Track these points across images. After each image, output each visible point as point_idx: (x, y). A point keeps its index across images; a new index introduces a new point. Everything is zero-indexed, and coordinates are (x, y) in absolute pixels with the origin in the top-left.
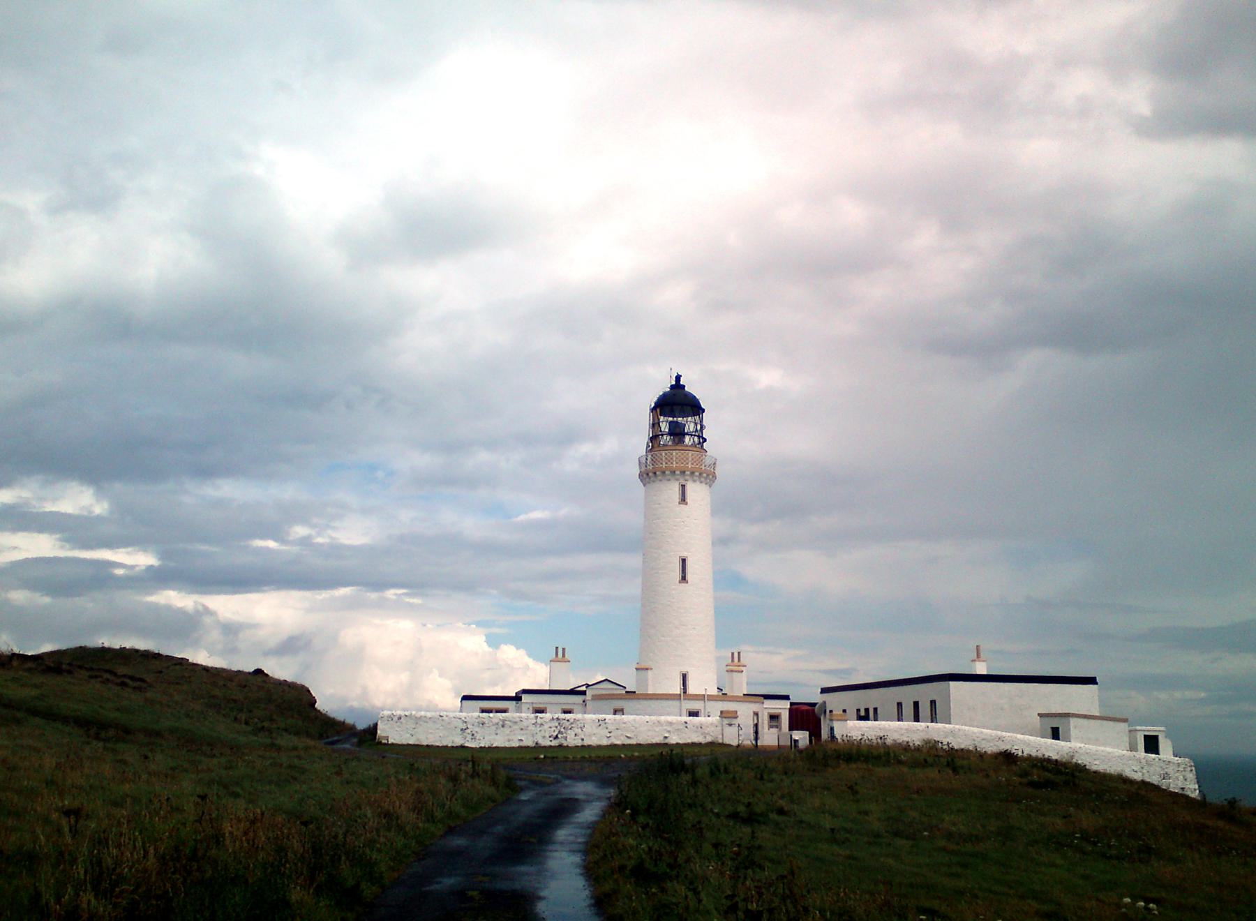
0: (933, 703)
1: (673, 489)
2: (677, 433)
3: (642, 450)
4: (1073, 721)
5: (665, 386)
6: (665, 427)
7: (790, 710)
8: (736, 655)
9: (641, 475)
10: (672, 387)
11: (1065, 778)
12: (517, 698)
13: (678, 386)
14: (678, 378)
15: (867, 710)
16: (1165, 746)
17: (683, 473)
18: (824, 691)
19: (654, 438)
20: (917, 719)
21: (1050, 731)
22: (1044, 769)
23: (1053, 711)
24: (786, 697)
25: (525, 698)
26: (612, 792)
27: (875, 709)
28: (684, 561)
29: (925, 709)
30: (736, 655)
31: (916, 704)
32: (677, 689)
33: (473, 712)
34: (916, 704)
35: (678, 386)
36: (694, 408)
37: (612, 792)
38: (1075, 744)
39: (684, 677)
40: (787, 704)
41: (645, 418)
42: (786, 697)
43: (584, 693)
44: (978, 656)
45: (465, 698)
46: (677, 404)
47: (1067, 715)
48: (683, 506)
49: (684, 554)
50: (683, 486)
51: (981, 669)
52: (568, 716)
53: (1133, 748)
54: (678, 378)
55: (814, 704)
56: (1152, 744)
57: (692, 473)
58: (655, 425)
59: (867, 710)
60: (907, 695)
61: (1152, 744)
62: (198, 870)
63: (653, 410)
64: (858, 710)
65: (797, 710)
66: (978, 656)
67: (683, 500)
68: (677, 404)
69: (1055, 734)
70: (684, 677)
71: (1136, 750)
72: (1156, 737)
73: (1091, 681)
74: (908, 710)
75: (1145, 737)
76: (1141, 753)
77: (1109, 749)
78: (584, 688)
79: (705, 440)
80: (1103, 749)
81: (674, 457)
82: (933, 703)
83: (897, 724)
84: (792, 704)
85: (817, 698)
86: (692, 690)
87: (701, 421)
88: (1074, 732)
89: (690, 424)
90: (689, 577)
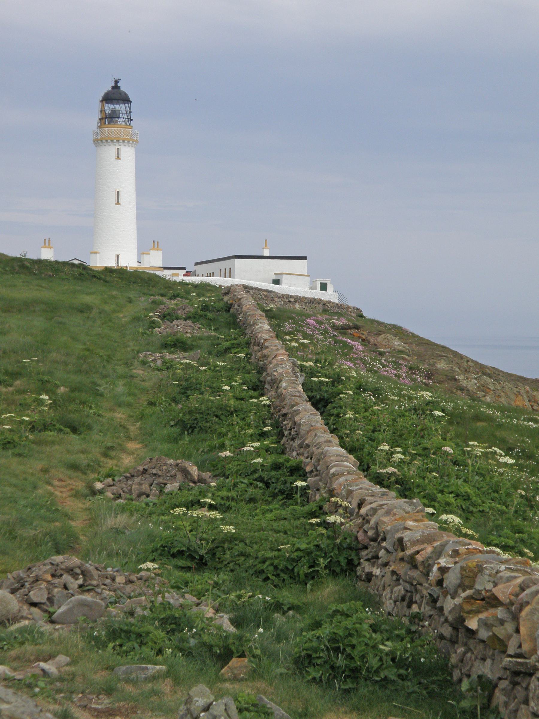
1: (111, 150)
4: (284, 276)
8: (47, 241)
9: (94, 141)
10: (113, 88)
13: (116, 87)
14: (116, 82)
16: (330, 287)
17: (118, 141)
18: (196, 264)
24: (184, 268)
27: (49, 240)
28: (118, 192)
30: (47, 241)
35: (116, 87)
36: (126, 100)
39: (118, 257)
42: (184, 268)
44: (266, 246)
46: (115, 96)
47: (282, 274)
48: (118, 160)
49: (118, 188)
50: (118, 149)
51: (266, 253)
52: (307, 415)
56: (324, 287)
57: (124, 141)
61: (324, 287)
63: (102, 101)
66: (266, 246)
67: (118, 157)
68: (115, 96)
70: (118, 257)
71: (316, 289)
73: (305, 258)
76: (318, 290)
77: (299, 289)
81: (111, 131)
87: (130, 108)
88: (236, 272)
89: (121, 107)
90: (121, 201)
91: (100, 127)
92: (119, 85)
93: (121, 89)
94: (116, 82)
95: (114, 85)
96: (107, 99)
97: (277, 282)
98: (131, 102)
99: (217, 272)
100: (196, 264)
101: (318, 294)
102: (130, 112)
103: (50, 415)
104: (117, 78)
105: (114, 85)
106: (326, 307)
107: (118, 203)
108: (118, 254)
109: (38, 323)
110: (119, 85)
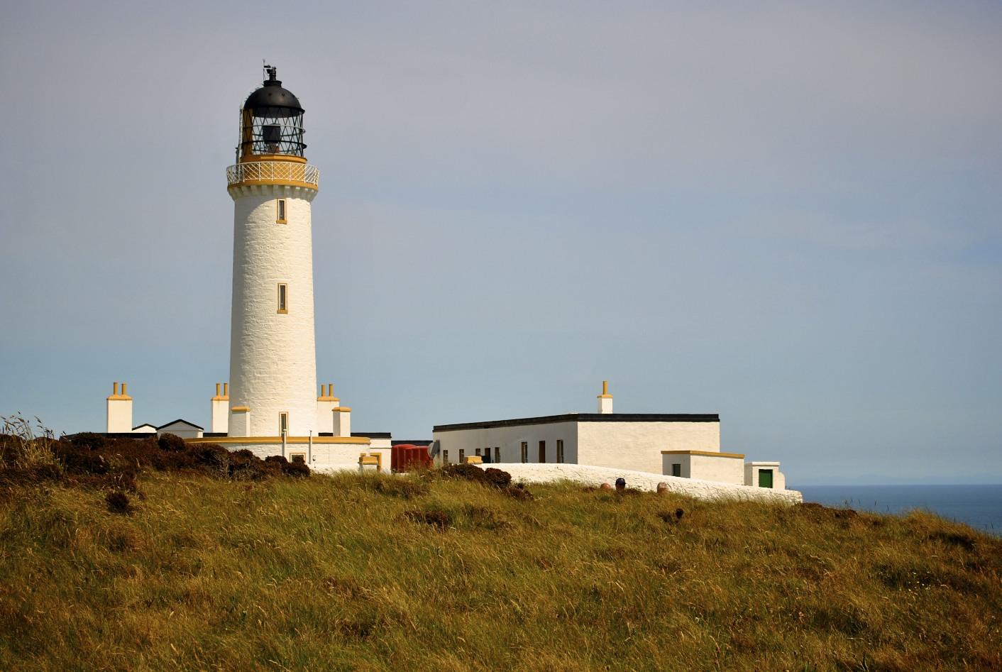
1: (270, 208)
2: (272, 136)
3: (231, 159)
4: (692, 458)
5: (257, 82)
7: (394, 451)
9: (230, 187)
10: (266, 83)
11: (680, 515)
13: (272, 83)
15: (488, 450)
16: (779, 480)
19: (246, 144)
20: (542, 460)
21: (671, 468)
22: (498, 475)
23: (705, 457)
24: (387, 436)
27: (497, 449)
29: (551, 449)
31: (542, 444)
32: (275, 432)
34: (542, 444)
35: (272, 83)
36: (294, 109)
40: (387, 443)
42: (387, 436)
46: (270, 103)
47: (688, 452)
49: (283, 281)
50: (282, 203)
51: (607, 407)
53: (748, 481)
54: (272, 72)
55: (428, 443)
58: (247, 128)
59: (488, 450)
60: (532, 435)
61: (766, 478)
62: (656, 619)
65: (401, 450)
67: (282, 217)
68: (270, 103)
70: (284, 417)
72: (770, 472)
73: (714, 418)
74: (534, 450)
75: (761, 471)
79: (305, 146)
80: (716, 479)
84: (393, 443)
85: (429, 436)
86: (292, 431)
89: (286, 125)
91: (243, 159)
93: (283, 86)
95: (268, 79)
96: (257, 104)
97: (677, 471)
98: (303, 111)
101: (755, 490)
102: (301, 131)
106: (779, 514)
107: (283, 306)
108: (283, 411)
110: (278, 78)
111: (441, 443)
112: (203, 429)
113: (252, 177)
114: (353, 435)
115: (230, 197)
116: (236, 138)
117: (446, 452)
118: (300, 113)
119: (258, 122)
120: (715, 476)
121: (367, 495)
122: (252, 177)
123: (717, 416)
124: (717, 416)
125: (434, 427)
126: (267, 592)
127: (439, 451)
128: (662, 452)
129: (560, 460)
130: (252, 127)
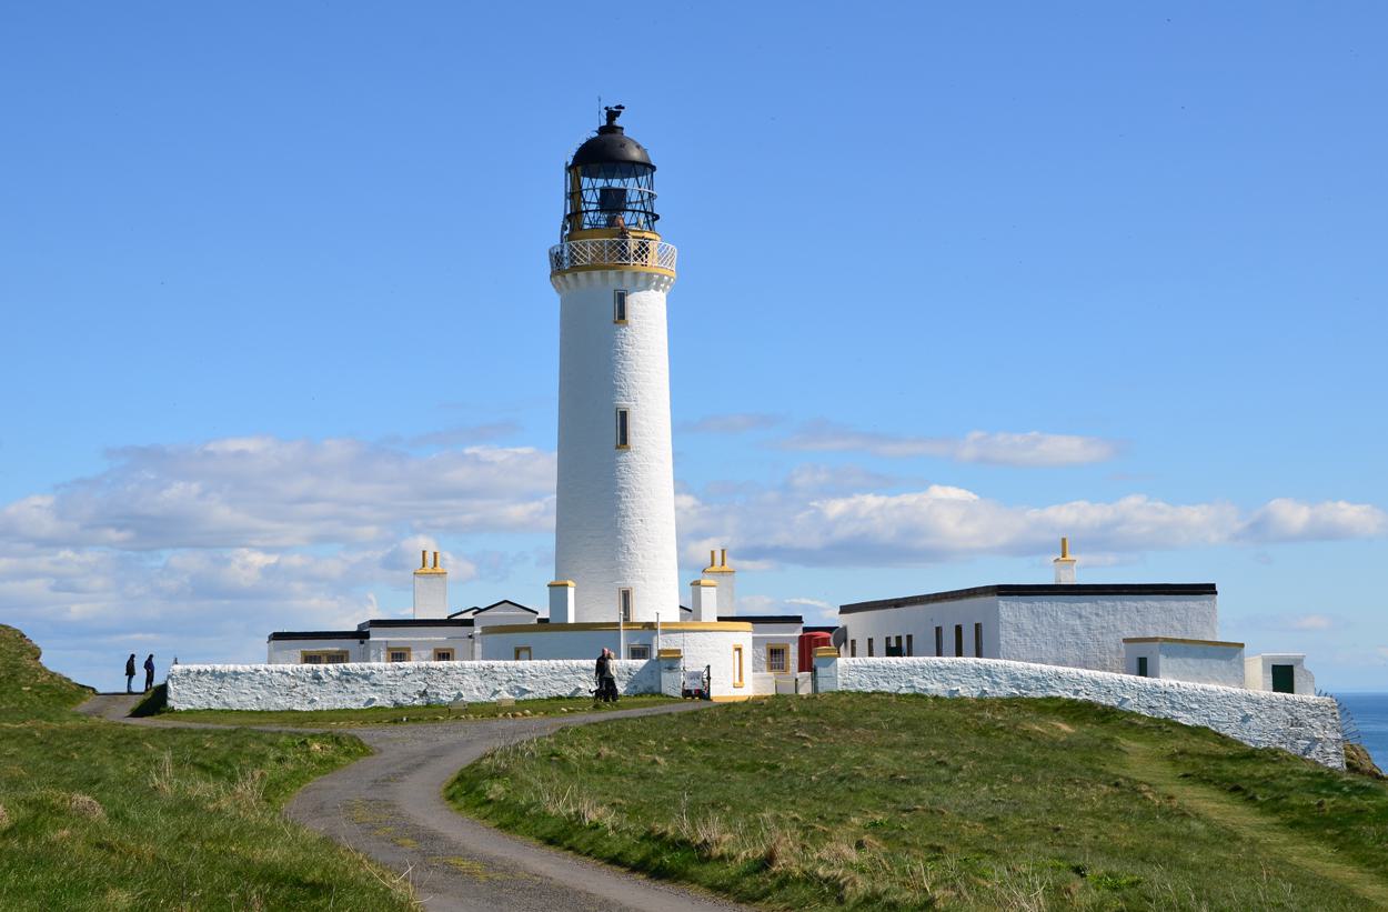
0: (978, 626)
2: (613, 202)
5: (589, 131)
6: (591, 198)
10: (602, 130)
12: (361, 635)
13: (609, 129)
14: (612, 115)
15: (899, 639)
18: (845, 610)
19: (574, 217)
20: (959, 653)
24: (798, 620)
25: (377, 637)
26: (710, 811)
27: (909, 638)
31: (959, 629)
33: (291, 664)
34: (959, 629)
35: (609, 129)
37: (710, 811)
38: (1164, 681)
41: (559, 184)
43: (470, 623)
45: (277, 636)
58: (575, 195)
59: (899, 639)
64: (888, 639)
68: (603, 155)
69: (1143, 668)
78: (469, 616)
82: (978, 626)
83: (936, 659)
88: (1007, 635)
89: (632, 186)
91: (570, 237)
92: (618, 122)
93: (626, 133)
94: (612, 115)
95: (604, 123)
98: (653, 168)
99: (924, 636)
100: (845, 610)
103: (748, 748)
104: (612, 105)
105: (604, 123)
109: (31, 812)
110: (618, 122)
111: (848, 629)
112: (537, 613)
113: (579, 260)
114: (720, 619)
115: (554, 290)
116: (558, 207)
117: (853, 642)
118: (649, 170)
119: (592, 187)
120: (1199, 674)
121: (554, 702)
122: (579, 260)
123: (1213, 586)
124: (1213, 586)
125: (841, 607)
126: (915, 753)
127: (846, 641)
128: (1124, 640)
129: (979, 654)
130: (581, 192)
